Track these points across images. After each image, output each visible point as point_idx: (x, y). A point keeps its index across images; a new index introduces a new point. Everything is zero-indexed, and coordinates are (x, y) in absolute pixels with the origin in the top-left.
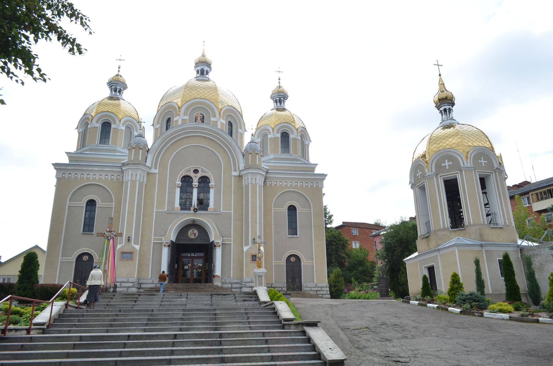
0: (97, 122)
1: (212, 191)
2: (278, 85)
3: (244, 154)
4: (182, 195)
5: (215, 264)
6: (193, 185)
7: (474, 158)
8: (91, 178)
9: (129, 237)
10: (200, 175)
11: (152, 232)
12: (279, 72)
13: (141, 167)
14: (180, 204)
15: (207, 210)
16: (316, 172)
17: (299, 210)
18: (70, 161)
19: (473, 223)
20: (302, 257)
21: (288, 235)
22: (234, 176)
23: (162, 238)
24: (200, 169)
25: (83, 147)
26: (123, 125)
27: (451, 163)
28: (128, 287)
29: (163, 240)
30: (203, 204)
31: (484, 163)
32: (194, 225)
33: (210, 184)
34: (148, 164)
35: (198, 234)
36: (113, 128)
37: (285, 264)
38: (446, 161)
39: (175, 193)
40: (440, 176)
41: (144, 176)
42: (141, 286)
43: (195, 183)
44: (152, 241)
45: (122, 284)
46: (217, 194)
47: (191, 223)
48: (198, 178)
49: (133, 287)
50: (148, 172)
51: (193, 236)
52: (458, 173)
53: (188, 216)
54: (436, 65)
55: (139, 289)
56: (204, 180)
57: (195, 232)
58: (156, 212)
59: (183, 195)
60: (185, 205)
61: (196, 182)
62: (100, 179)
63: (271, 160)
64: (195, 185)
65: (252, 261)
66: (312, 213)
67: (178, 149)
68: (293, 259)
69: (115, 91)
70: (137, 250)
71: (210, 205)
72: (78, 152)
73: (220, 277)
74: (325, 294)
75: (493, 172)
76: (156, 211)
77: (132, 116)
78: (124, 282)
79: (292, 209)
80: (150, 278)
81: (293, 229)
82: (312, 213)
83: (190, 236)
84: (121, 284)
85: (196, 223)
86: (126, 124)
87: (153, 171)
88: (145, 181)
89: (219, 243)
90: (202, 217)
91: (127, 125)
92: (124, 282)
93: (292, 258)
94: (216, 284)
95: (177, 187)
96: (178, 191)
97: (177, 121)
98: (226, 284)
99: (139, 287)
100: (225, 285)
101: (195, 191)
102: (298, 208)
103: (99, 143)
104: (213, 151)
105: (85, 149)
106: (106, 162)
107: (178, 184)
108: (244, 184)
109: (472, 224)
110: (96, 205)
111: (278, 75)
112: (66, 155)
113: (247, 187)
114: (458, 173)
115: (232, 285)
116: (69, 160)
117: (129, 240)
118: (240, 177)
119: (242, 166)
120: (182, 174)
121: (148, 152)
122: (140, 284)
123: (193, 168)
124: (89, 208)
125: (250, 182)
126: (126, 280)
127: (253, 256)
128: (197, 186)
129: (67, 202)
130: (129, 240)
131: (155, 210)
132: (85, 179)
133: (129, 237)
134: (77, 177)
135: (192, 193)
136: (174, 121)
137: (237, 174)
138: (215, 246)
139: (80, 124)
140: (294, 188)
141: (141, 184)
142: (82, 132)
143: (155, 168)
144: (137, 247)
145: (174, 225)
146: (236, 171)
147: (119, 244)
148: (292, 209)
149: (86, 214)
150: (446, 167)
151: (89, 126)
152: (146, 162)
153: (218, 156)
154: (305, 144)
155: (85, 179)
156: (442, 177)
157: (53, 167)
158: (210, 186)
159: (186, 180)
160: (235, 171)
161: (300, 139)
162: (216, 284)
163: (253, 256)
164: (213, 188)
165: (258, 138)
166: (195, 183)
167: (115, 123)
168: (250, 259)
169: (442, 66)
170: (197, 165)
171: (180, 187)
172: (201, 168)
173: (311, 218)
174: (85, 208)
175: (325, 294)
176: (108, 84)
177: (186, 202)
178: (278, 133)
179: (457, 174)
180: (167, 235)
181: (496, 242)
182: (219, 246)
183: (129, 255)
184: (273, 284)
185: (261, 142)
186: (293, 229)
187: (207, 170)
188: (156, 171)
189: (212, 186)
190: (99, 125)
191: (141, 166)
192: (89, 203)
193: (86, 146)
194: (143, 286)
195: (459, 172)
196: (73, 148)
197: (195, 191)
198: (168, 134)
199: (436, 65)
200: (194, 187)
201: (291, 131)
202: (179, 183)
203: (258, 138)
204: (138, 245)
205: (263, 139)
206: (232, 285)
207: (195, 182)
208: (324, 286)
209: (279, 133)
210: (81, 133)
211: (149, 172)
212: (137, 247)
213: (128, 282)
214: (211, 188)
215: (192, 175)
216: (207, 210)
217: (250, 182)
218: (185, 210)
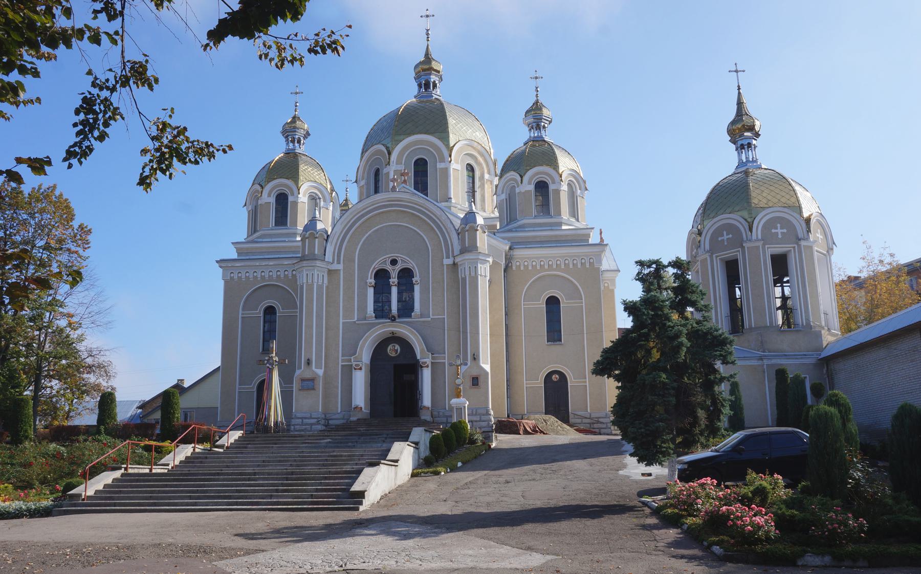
0: (269, 195)
1: (417, 289)
2: (534, 100)
3: (459, 231)
4: (378, 296)
5: (422, 392)
6: (391, 283)
7: (764, 227)
8: (267, 276)
9: (308, 360)
10: (399, 267)
11: (339, 350)
12: (536, 78)
13: (318, 263)
14: (375, 311)
15: (410, 316)
16: (590, 242)
17: (280, 312)
18: (239, 254)
19: (754, 325)
20: (569, 375)
21: (547, 342)
22: (447, 265)
23: (351, 359)
24: (400, 258)
25: (255, 231)
26: (304, 195)
27: (730, 236)
28: (312, 424)
29: (352, 361)
30: (406, 309)
31: (727, 235)
32: (394, 338)
33: (413, 279)
34: (329, 257)
35: (401, 350)
36: (291, 202)
37: (543, 385)
38: (725, 233)
39: (366, 296)
40: (717, 257)
41: (323, 275)
42: (328, 422)
43: (394, 280)
44: (340, 364)
45: (304, 420)
46: (425, 291)
47: (390, 335)
48: (398, 271)
49: (318, 423)
50: (328, 269)
51: (394, 353)
52: (739, 251)
53: (385, 328)
54: (733, 71)
55: (326, 426)
56: (406, 275)
57: (396, 348)
58: (343, 323)
59: (379, 297)
60: (382, 311)
61: (395, 278)
62: (278, 277)
63: (520, 228)
64: (393, 282)
65: (473, 385)
66: (584, 307)
67: (367, 233)
68: (555, 377)
69: (293, 141)
70: (319, 376)
71: (415, 308)
72: (251, 238)
73: (430, 409)
74: (604, 428)
75: (796, 245)
76: (343, 322)
77: (318, 181)
78: (306, 418)
79: (553, 303)
80: (339, 412)
81: (554, 333)
82: (584, 307)
83: (390, 354)
84: (302, 421)
85: (397, 335)
86: (311, 193)
87: (335, 266)
88: (326, 281)
89: (426, 363)
90: (402, 329)
91: (312, 194)
92: (306, 418)
93: (554, 376)
94: (423, 418)
95: (370, 286)
96: (371, 292)
97: (388, 173)
98: (439, 417)
99: (326, 424)
100: (439, 419)
101: (394, 290)
102: (563, 299)
103: (274, 225)
104: (415, 231)
105: (257, 234)
106: (286, 252)
107: (370, 283)
108: (460, 276)
109: (753, 326)
110: (276, 314)
111: (533, 83)
112: (232, 246)
113: (464, 279)
114: (739, 251)
115: (480, 417)
116: (238, 253)
117: (308, 364)
118: (455, 264)
119: (457, 248)
120: (374, 268)
121: (327, 241)
122: (328, 420)
123: (389, 257)
124: (268, 317)
125: (467, 273)
126: (309, 415)
127: (473, 378)
128: (396, 283)
129: (240, 316)
130: (309, 362)
131: (341, 321)
132: (260, 279)
133: (308, 360)
134: (249, 276)
135: (391, 293)
136: (384, 173)
137: (448, 262)
138: (422, 367)
139: (248, 199)
140: (555, 270)
141: (320, 287)
142: (253, 210)
143: (339, 262)
144: (320, 372)
145: (366, 340)
146: (449, 258)
147: (298, 369)
148: (553, 303)
149: (264, 326)
150: (781, 226)
151: (260, 202)
152: (325, 255)
153: (421, 236)
154: (576, 197)
155: (260, 279)
156: (718, 258)
157: (217, 265)
158: (414, 282)
159: (381, 276)
160: (448, 257)
161: (566, 190)
162: (423, 418)
163: (473, 378)
164: (418, 284)
165: (502, 193)
166: (394, 280)
167: (293, 194)
168: (469, 382)
169: (744, 71)
170: (394, 253)
171: (373, 286)
172: (400, 257)
173: (583, 315)
174: (262, 318)
175: (604, 428)
176: (282, 133)
177: (383, 306)
178: (530, 183)
179: (738, 253)
180: (357, 354)
181: (788, 352)
182: (427, 366)
183: (310, 383)
184: (525, 415)
185: (506, 199)
186: (554, 333)
187: (408, 259)
188: (340, 267)
189: (416, 281)
190: (272, 200)
191: (317, 262)
192: (267, 311)
193: (258, 231)
194: (330, 422)
195: (740, 249)
196: (242, 235)
197: (394, 290)
198: (359, 207)
199: (733, 71)
200: (392, 285)
201: (550, 178)
202: (371, 281)
203: (502, 193)
204: (321, 369)
205: (509, 194)
206: (447, 420)
207: (393, 278)
208: (602, 416)
209: (532, 183)
210: (251, 212)
211: (330, 269)
212: (320, 372)
213: (311, 418)
214: (415, 284)
215: (389, 267)
216: (410, 316)
217: (467, 273)
218: (382, 318)
